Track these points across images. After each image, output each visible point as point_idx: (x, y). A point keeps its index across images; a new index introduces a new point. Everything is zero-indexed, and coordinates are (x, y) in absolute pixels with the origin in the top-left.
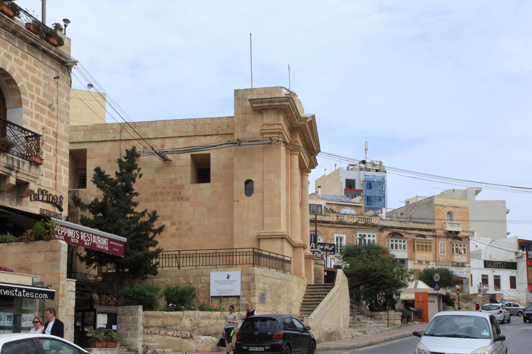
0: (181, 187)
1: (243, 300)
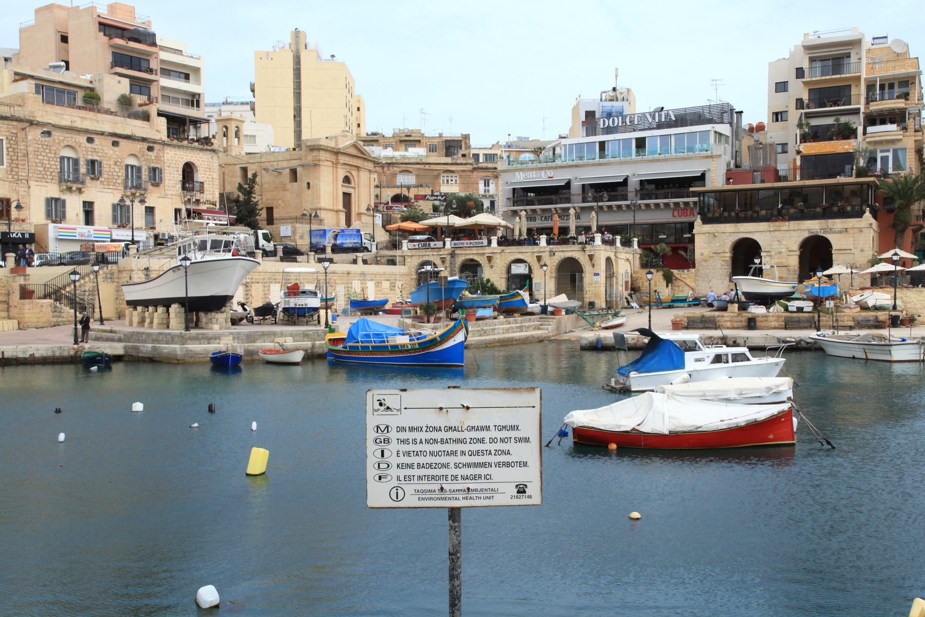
0: (285, 184)
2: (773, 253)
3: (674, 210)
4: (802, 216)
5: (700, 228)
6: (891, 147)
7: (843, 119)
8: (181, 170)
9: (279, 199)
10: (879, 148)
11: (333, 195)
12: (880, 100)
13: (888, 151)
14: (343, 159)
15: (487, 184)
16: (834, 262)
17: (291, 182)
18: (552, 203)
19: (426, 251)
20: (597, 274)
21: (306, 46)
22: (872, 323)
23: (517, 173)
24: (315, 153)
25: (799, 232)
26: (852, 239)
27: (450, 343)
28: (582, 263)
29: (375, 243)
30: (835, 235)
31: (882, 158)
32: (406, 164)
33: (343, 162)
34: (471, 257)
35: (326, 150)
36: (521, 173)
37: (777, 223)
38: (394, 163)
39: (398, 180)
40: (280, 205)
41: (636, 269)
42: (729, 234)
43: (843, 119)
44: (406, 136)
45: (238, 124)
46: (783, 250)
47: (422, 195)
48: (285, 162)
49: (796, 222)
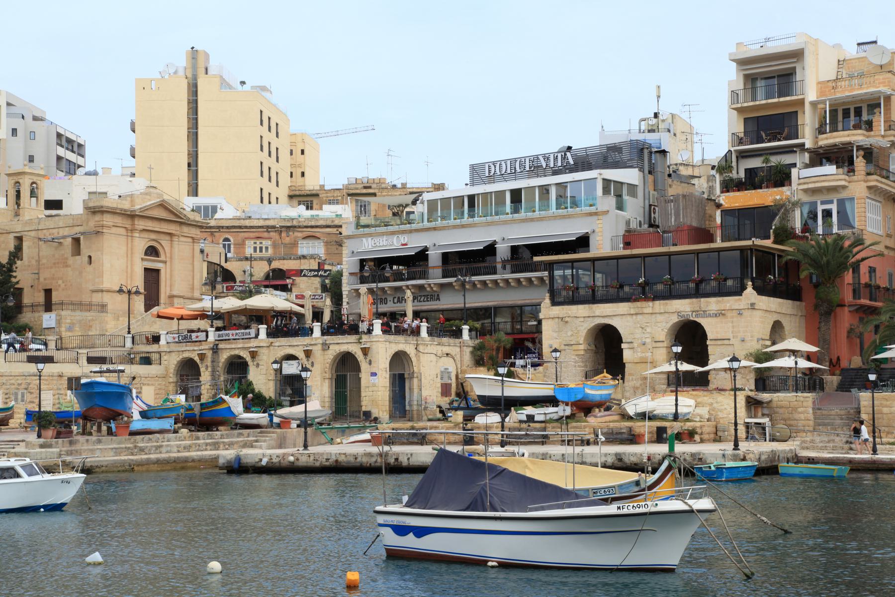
0: (67, 259)
1: (57, 330)
2: (635, 345)
4: (670, 295)
5: (548, 311)
6: (835, 197)
7: (775, 160)
9: (59, 279)
10: (818, 199)
11: (127, 272)
12: (830, 132)
13: (831, 202)
14: (141, 224)
16: (710, 357)
19: (186, 346)
20: (374, 374)
21: (207, 69)
22: (625, 436)
23: (364, 240)
24: (98, 217)
25: (667, 315)
26: (731, 324)
28: (359, 360)
29: (131, 335)
30: (710, 320)
31: (823, 211)
32: (312, 227)
33: (142, 227)
34: (236, 352)
35: (113, 212)
36: (370, 239)
37: (638, 304)
38: (295, 227)
39: (247, 251)
40: (59, 286)
41: (464, 368)
42: (582, 319)
43: (775, 160)
44: (365, 187)
46: (648, 340)
47: (296, 270)
48: (67, 229)
49: (662, 302)
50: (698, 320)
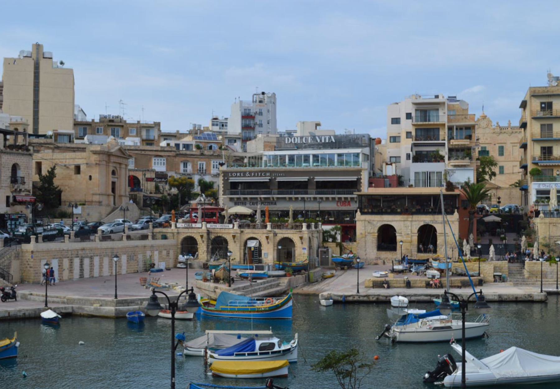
3: (338, 202)
4: (419, 212)
8: (10, 169)
14: (113, 159)
15: (185, 165)
17: (75, 174)
18: (258, 194)
27: (285, 307)
45: (25, 127)
50: (432, 224)
